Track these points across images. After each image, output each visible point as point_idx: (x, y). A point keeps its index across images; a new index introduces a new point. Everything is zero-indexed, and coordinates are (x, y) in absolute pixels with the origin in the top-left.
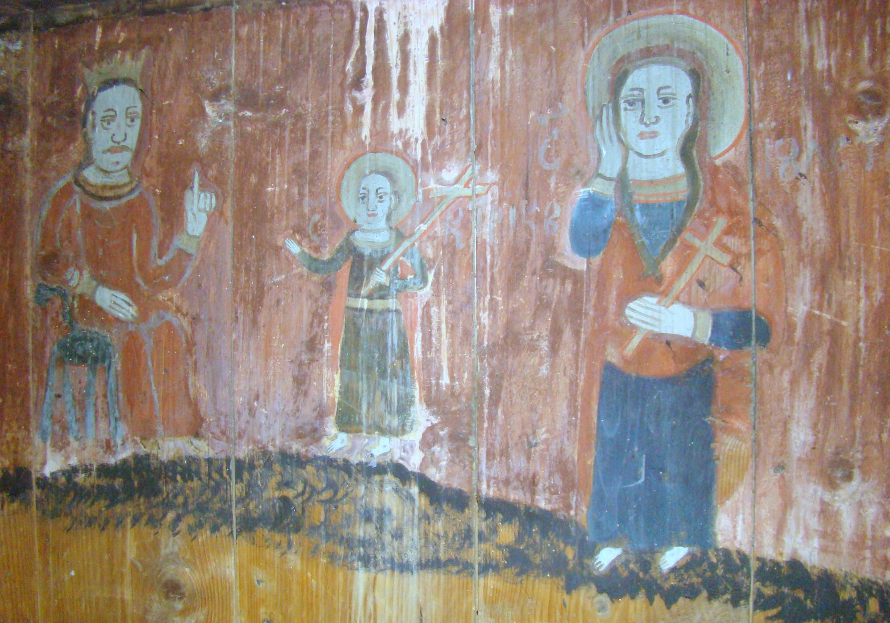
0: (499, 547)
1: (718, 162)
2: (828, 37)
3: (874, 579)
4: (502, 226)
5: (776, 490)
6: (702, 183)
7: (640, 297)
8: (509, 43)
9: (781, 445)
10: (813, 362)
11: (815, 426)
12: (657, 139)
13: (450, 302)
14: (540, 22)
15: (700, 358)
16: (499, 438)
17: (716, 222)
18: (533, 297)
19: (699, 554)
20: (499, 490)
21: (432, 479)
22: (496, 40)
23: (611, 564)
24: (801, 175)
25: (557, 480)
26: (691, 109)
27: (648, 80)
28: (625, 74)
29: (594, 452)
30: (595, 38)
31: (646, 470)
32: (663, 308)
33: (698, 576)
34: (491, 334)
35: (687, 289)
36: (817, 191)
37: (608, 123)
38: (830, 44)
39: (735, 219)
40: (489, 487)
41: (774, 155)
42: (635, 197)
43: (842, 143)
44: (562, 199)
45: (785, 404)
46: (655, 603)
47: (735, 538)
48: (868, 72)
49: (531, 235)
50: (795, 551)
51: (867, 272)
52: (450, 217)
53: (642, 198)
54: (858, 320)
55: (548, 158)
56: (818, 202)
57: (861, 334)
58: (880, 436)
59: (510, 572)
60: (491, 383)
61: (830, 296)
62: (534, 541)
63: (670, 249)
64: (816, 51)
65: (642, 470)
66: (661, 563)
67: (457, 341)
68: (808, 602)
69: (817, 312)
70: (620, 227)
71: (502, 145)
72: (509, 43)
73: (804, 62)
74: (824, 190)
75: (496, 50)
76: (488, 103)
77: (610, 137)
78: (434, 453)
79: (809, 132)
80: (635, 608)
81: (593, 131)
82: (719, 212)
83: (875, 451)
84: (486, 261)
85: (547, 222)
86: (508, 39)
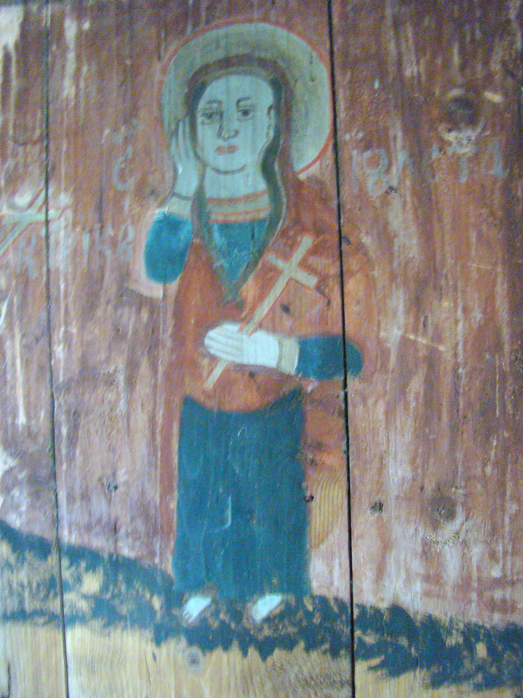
0: (85, 597)
1: (302, 177)
2: (417, 43)
3: (480, 624)
4: (76, 252)
5: (374, 531)
6: (285, 200)
7: (221, 325)
8: (84, 60)
9: (378, 483)
10: (410, 391)
11: (413, 461)
12: (237, 153)
13: (24, 336)
14: (117, 34)
15: (286, 389)
16: (78, 481)
17: (301, 242)
18: (109, 328)
19: (293, 603)
20: (81, 535)
21: (13, 526)
22: (71, 56)
23: (200, 614)
24: (391, 188)
25: (140, 525)
26: (273, 122)
27: (228, 92)
28: (203, 86)
29: (176, 494)
30: (172, 48)
31: (233, 514)
32: (245, 337)
33: (294, 624)
34: (67, 369)
35: (270, 316)
36: (409, 206)
37: (184, 137)
38: (420, 50)
39: (321, 238)
40: (70, 532)
41: (362, 168)
42: (213, 217)
43: (435, 155)
44: (136, 220)
45: (382, 437)
46: (249, 655)
47: (332, 583)
48: (459, 80)
49: (105, 260)
50: (396, 596)
51: (464, 292)
52: (22, 244)
53: (221, 218)
54: (457, 345)
55: (122, 176)
56: (410, 216)
57: (460, 359)
58: (483, 471)
59: (97, 623)
60: (68, 420)
61: (426, 318)
62: (120, 591)
63: (252, 270)
64: (405, 58)
65: (229, 513)
66: (253, 613)
67: (33, 377)
68: (413, 650)
69: (412, 337)
70: (197, 249)
71: (76, 167)
72: (84, 60)
73: (392, 69)
74: (416, 205)
75: (71, 66)
76: (62, 123)
77: (187, 153)
78: (13, 497)
79: (399, 143)
80: (228, 661)
81: (168, 147)
82: (304, 230)
83: (479, 486)
84: (59, 291)
85: (122, 246)
86: (83, 55)
